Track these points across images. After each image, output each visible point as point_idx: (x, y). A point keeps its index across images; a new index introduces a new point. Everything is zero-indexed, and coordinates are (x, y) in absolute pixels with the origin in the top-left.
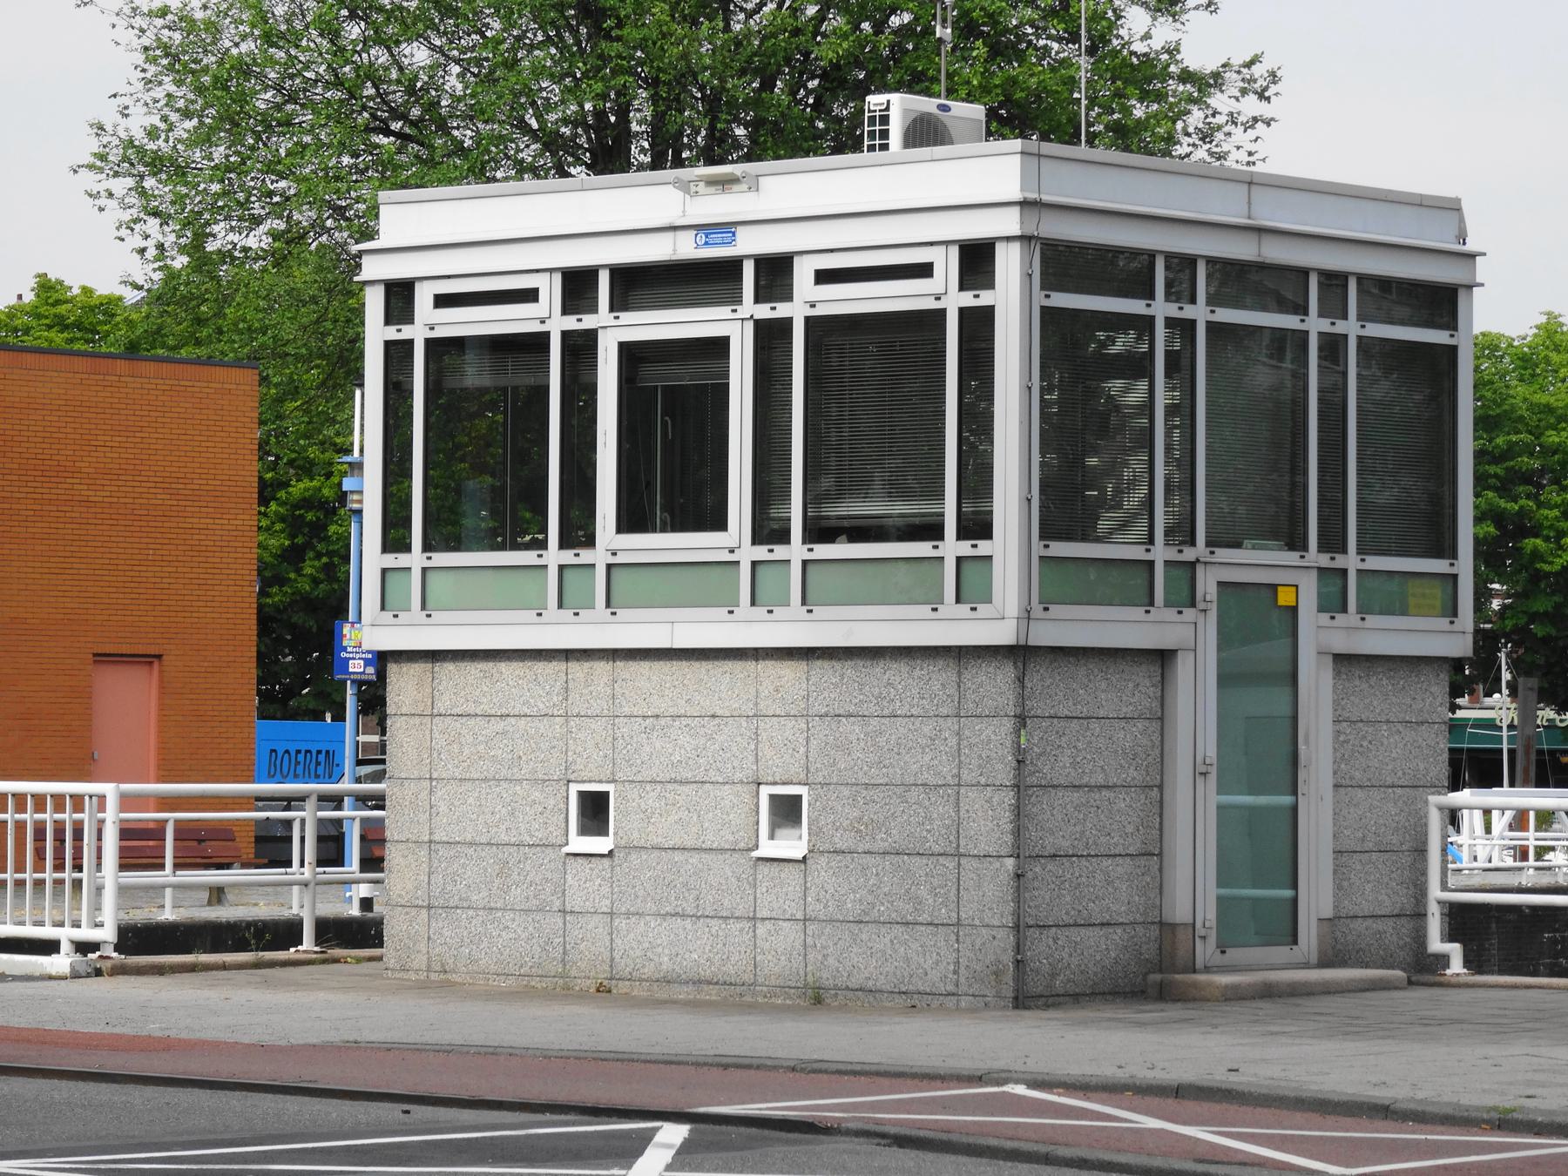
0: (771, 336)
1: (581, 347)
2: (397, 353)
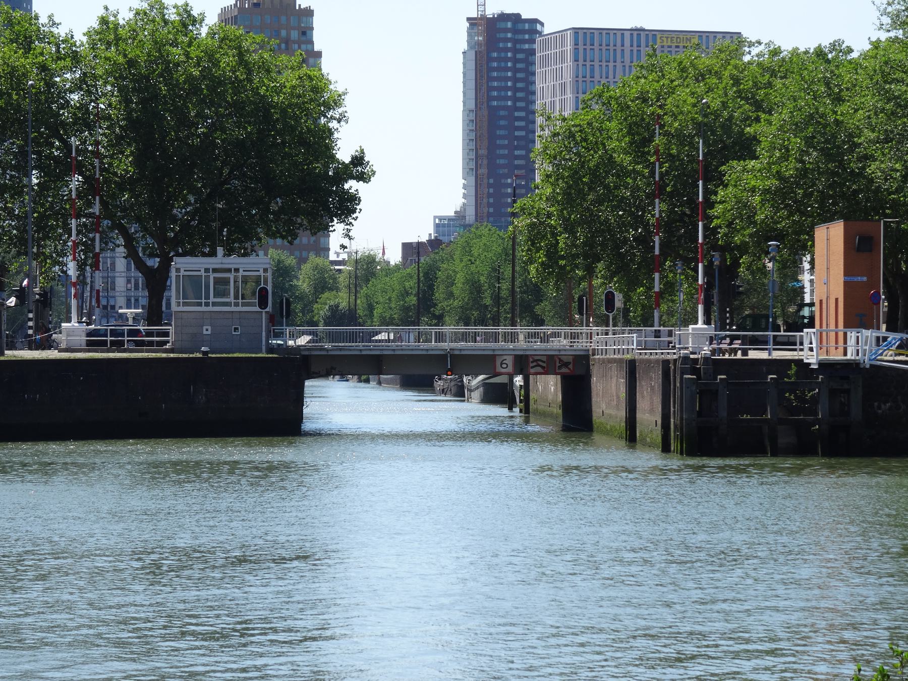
0: (207, 297)
1: (207, 277)
2: (178, 277)
